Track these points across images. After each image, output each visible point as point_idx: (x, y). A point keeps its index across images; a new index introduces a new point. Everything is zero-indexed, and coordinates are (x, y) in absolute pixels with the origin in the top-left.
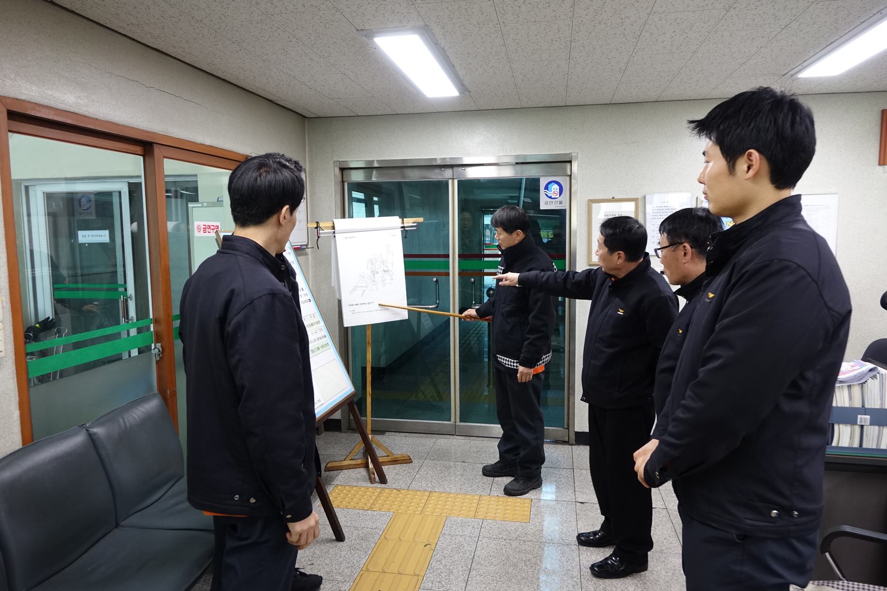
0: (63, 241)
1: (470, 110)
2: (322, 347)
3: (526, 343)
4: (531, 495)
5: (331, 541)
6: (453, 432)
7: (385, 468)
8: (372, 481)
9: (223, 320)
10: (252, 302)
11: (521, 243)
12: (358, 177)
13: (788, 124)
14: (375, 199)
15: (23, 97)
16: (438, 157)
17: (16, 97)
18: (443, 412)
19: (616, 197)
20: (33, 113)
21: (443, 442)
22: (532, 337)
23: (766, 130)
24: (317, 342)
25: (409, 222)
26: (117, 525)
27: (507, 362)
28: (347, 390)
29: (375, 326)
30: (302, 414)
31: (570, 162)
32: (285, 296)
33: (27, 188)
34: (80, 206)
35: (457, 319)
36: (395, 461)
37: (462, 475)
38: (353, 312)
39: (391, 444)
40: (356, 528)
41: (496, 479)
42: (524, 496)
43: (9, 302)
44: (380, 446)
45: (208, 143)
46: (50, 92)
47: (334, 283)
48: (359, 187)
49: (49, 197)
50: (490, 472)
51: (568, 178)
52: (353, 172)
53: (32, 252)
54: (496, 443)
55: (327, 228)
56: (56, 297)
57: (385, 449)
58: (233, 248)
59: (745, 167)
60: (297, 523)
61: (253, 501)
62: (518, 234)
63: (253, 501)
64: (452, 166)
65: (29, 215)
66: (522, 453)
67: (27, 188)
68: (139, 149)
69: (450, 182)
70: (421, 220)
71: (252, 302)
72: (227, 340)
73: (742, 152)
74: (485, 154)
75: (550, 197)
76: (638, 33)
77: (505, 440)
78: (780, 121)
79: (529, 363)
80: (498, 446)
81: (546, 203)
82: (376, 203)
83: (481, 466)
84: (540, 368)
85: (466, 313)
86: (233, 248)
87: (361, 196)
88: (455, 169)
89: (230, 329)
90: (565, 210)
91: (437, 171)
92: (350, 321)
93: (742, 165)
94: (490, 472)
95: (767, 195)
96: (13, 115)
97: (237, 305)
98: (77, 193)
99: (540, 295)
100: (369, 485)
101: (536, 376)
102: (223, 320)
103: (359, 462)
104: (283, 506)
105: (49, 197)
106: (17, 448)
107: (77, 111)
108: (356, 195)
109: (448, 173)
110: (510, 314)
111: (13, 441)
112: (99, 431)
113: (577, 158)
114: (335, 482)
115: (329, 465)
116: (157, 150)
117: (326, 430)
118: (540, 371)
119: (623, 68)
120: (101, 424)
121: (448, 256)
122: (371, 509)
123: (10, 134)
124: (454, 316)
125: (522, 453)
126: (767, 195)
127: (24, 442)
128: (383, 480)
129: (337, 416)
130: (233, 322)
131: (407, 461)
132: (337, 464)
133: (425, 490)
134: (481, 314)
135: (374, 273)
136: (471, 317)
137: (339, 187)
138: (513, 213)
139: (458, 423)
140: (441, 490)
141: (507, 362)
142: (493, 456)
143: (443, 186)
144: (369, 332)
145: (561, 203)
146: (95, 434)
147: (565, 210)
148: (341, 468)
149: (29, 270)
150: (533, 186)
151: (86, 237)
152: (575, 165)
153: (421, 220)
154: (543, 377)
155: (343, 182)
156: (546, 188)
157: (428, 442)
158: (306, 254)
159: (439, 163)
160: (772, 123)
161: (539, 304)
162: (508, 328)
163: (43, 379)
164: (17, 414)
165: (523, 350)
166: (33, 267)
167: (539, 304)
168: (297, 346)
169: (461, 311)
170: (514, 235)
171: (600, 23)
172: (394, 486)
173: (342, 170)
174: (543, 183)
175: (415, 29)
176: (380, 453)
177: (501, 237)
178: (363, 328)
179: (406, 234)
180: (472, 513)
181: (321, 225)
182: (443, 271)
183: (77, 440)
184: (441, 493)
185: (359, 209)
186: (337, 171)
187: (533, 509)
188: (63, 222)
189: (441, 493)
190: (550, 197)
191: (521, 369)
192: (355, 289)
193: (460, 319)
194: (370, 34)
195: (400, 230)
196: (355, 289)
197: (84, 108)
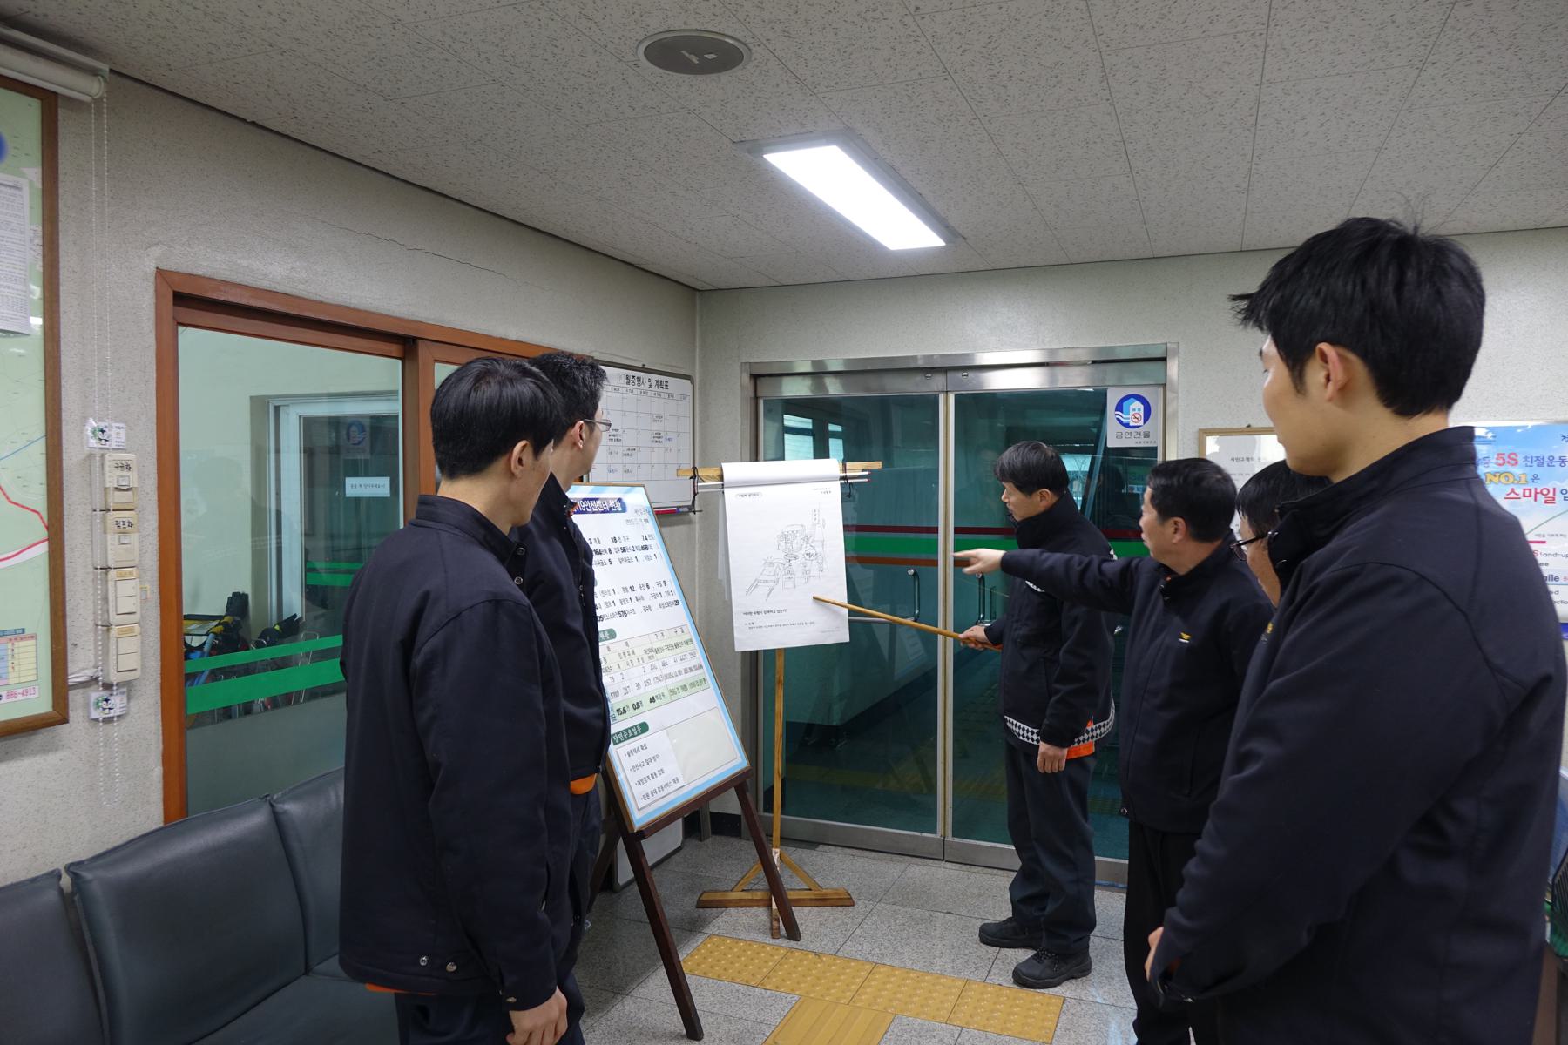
0: (321, 493)
1: (960, 273)
2: (693, 685)
3: (1054, 699)
4: (1066, 990)
5: (678, 1037)
6: (940, 855)
7: (799, 913)
8: (775, 934)
9: (408, 645)
10: (459, 615)
11: (1049, 512)
12: (797, 389)
13: (1389, 288)
14: (832, 428)
15: (200, 272)
16: (919, 354)
17: (189, 271)
18: (922, 814)
19: (1254, 425)
20: (215, 296)
21: (919, 872)
22: (1065, 688)
23: (1383, 305)
24: (690, 674)
25: (857, 469)
26: (307, 970)
27: (1024, 732)
28: (734, 763)
29: (789, 652)
30: (541, 814)
31: (1164, 359)
32: (518, 604)
33: (277, 409)
34: (349, 437)
35: (950, 641)
36: (822, 901)
37: (942, 938)
38: (752, 626)
39: (832, 867)
40: (727, 1018)
41: (1005, 951)
42: (1051, 991)
43: (156, 590)
44: (796, 869)
45: (513, 337)
46: (245, 263)
47: (721, 575)
48: (796, 406)
49: (309, 424)
50: (994, 936)
51: (1161, 389)
52: (786, 380)
53: (279, 513)
54: (1007, 879)
55: (711, 478)
56: (311, 582)
57: (806, 877)
58: (432, 517)
59: (1321, 376)
60: (527, 1013)
61: (451, 967)
62: (1042, 497)
63: (451, 967)
64: (944, 370)
65: (278, 451)
66: (1050, 908)
67: (277, 409)
68: (394, 348)
69: (942, 397)
70: (877, 465)
71: (459, 615)
72: (413, 681)
73: (1310, 349)
74: (1012, 351)
75: (1127, 425)
76: (1251, 120)
77: (1025, 876)
78: (1372, 282)
79: (1061, 736)
80: (1011, 888)
81: (1119, 436)
82: (835, 435)
83: (979, 923)
84: (1085, 745)
85: (968, 633)
86: (432, 517)
87: (806, 423)
88: (950, 375)
89: (418, 661)
90: (1155, 449)
91: (919, 378)
92: (748, 638)
93: (1315, 374)
94: (994, 936)
95: (1380, 433)
96: (181, 299)
97: (432, 619)
98: (345, 417)
99: (1081, 610)
100: (769, 940)
101: (1076, 763)
102: (408, 645)
103: (759, 895)
104: (502, 982)
105: (309, 424)
106: (154, 827)
107: (288, 290)
108: (790, 421)
109: (937, 382)
110: (1027, 642)
111: (150, 815)
112: (292, 808)
113: (1176, 352)
114: (710, 930)
115: (704, 897)
116: (423, 351)
117: (714, 833)
118: (1085, 752)
119: (1245, 185)
120: (296, 798)
121: (936, 530)
122: (761, 985)
123: (180, 329)
124: (946, 635)
125: (1050, 908)
126: (1380, 433)
127: (167, 817)
128: (793, 933)
129: (731, 805)
130: (427, 648)
131: (845, 901)
132: (718, 896)
133: (866, 961)
134: (994, 636)
135: (791, 557)
136: (977, 641)
137: (748, 409)
138: (1033, 457)
139: (950, 838)
140: (896, 963)
141: (1024, 732)
142: (1001, 911)
143: (931, 403)
144: (780, 663)
145: (1147, 435)
146: (285, 812)
147: (1155, 449)
148: (723, 904)
149: (274, 536)
150: (1094, 403)
151: (359, 487)
152: (1173, 368)
153: (877, 465)
154: (1092, 764)
155: (756, 398)
156: (1119, 407)
157: (891, 870)
158: (690, 522)
159: (921, 364)
160: (1358, 288)
161: (1078, 627)
162: (1024, 667)
163: (200, 720)
164: (157, 772)
165: (1048, 712)
166: (279, 531)
167: (1078, 627)
168: (537, 693)
169: (960, 627)
170: (1037, 497)
171: (1167, 106)
172: (812, 947)
173: (755, 377)
174: (1112, 399)
175: (827, 137)
176: (792, 885)
177: (1013, 499)
178: (770, 654)
179: (850, 491)
180: (945, 1013)
181: (701, 473)
182: (923, 556)
183: (257, 819)
184: (894, 968)
185: (798, 446)
186: (746, 379)
187: (1063, 1018)
188: (323, 462)
189: (894, 968)
190: (1127, 425)
191: (1043, 747)
192: (755, 585)
193: (956, 641)
194: (757, 147)
195: (837, 484)
196: (755, 585)
197: (301, 286)
